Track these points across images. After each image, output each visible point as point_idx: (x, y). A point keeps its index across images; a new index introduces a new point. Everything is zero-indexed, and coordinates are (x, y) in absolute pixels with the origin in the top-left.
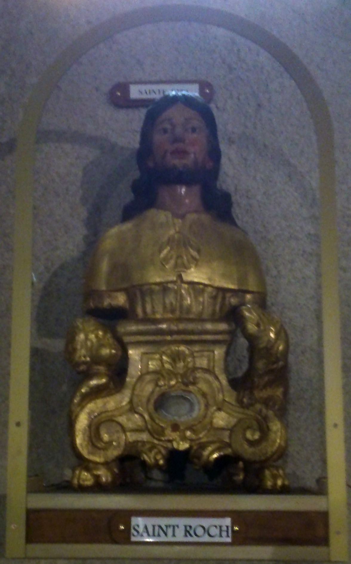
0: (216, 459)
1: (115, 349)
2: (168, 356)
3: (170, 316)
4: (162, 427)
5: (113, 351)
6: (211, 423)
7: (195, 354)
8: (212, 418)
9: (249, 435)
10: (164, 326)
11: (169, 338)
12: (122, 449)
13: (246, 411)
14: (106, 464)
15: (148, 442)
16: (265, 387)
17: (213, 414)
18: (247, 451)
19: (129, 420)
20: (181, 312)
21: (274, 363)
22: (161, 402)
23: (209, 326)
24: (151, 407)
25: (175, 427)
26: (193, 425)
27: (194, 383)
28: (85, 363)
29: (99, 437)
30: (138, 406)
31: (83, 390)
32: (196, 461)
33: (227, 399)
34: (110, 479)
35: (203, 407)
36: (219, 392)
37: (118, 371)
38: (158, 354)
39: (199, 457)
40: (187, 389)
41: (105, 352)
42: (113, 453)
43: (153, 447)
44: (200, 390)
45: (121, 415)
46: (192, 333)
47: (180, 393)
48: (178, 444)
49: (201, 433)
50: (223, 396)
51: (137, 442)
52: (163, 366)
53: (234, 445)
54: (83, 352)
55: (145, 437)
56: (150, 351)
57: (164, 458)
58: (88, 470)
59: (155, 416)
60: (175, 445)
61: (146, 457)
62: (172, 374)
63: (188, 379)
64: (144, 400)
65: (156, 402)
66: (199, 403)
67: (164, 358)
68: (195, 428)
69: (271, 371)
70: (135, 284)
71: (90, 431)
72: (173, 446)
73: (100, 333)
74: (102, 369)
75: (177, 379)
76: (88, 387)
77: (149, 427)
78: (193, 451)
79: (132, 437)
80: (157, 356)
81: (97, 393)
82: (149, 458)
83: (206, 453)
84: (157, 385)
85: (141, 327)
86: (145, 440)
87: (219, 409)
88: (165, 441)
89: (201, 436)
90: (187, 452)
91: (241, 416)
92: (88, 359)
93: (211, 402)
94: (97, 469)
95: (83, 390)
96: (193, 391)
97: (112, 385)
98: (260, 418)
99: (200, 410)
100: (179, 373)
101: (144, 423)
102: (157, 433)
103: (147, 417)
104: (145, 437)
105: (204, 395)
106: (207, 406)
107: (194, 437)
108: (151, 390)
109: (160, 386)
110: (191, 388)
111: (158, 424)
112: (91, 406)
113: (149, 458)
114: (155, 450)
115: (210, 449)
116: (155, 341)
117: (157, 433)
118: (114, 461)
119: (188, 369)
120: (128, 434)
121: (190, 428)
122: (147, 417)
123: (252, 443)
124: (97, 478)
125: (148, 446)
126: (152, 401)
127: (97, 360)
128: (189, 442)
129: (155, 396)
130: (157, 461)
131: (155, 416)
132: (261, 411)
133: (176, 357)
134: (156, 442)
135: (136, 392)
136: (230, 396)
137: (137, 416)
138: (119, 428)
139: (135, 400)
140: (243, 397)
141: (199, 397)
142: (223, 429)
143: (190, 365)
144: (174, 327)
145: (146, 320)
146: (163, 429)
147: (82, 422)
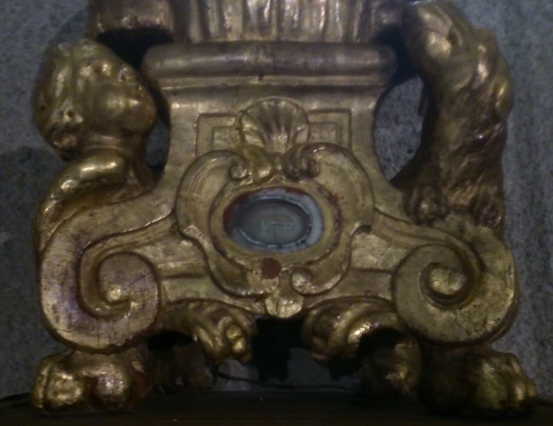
0: (364, 337)
1: (137, 97)
2: (251, 118)
3: (257, 37)
4: (241, 267)
5: (134, 102)
6: (348, 258)
7: (312, 118)
8: (350, 248)
9: (439, 283)
10: (245, 57)
11: (255, 81)
12: (151, 316)
13: (431, 233)
14: (113, 351)
15: (211, 301)
16: (460, 184)
17: (352, 237)
18: (439, 321)
19: (167, 252)
20: (280, 29)
21: (486, 125)
22: (239, 213)
23: (341, 59)
24: (217, 223)
25: (271, 268)
26: (310, 263)
27: (310, 174)
28: (71, 129)
29: (98, 289)
30: (188, 223)
31: (65, 185)
32: (317, 341)
33: (382, 208)
34: (122, 386)
35: (330, 223)
36: (364, 193)
37: (147, 155)
38: (235, 116)
39: (325, 334)
40: (295, 186)
41: (117, 103)
42: (128, 325)
43: (223, 310)
44: (321, 188)
45: (151, 243)
46: (306, 71)
47: (280, 194)
48: (278, 305)
49: (328, 279)
50: (374, 201)
51: (183, 302)
52: (243, 139)
53: (401, 305)
54: (68, 106)
55: (203, 289)
56: (216, 111)
57: (244, 334)
58: (68, 365)
59: (226, 243)
60: (270, 308)
61: (204, 336)
62: (263, 156)
63: (299, 166)
64: (203, 210)
65: (228, 212)
66: (322, 216)
67: (247, 126)
68: (312, 267)
69: (477, 145)
70: (214, 149)
71: (77, 277)
72: (265, 307)
73: (106, 67)
74: (110, 140)
75: (273, 164)
76: (75, 178)
77: (213, 267)
78: (309, 321)
79: (173, 291)
80: (231, 122)
81: (98, 190)
82: (212, 337)
83: (340, 324)
84: (231, 178)
85: (199, 60)
86: (203, 296)
87: (366, 229)
88: (247, 296)
89: (329, 285)
90: (297, 320)
91: (413, 242)
92: (79, 119)
93: (347, 213)
94: (93, 364)
95: (65, 185)
96: (307, 190)
97: (132, 179)
98: (459, 244)
99: (323, 229)
100: (278, 154)
101: (202, 262)
102: (229, 280)
103: (207, 244)
104: (203, 289)
105: (332, 199)
106: (339, 221)
107: (313, 289)
108: (217, 188)
109: (238, 180)
110: (302, 184)
111: (231, 261)
112: (80, 220)
113: (209, 337)
114: (227, 319)
115: (349, 314)
116: (229, 83)
117: (229, 280)
118: (128, 344)
119: (296, 146)
120: (166, 284)
121: (305, 270)
122: (207, 244)
123: (445, 301)
124: (91, 384)
125: (209, 309)
126: (220, 212)
127: (98, 121)
128: (301, 299)
129: (225, 203)
130: (229, 344)
131: (226, 243)
132: (462, 230)
133: (269, 123)
134: (227, 300)
135: (184, 193)
136: (388, 203)
137: (185, 243)
138: (144, 270)
139: (182, 209)
140: (420, 200)
141: (322, 202)
142: (373, 271)
143: (302, 138)
144: (264, 59)
145: (209, 45)
146: (244, 271)
147: (58, 253)
